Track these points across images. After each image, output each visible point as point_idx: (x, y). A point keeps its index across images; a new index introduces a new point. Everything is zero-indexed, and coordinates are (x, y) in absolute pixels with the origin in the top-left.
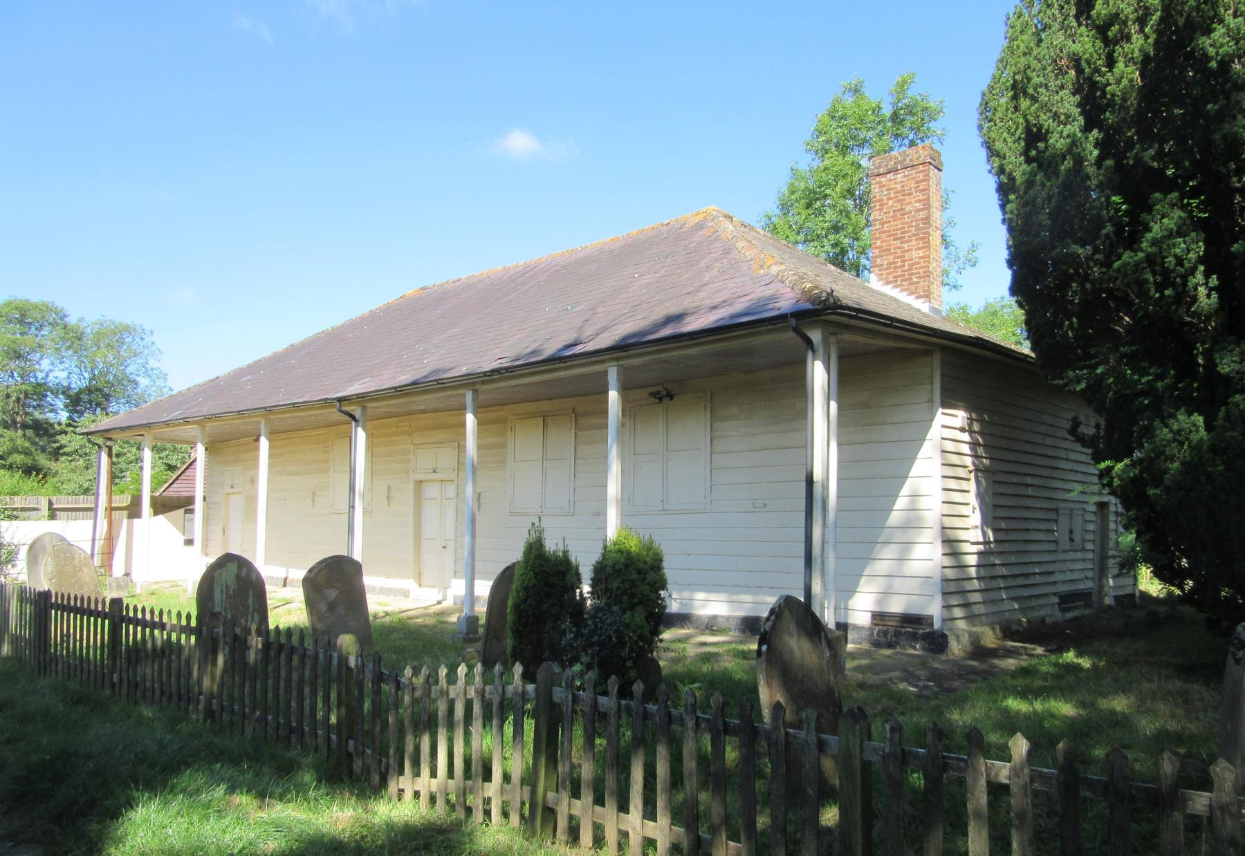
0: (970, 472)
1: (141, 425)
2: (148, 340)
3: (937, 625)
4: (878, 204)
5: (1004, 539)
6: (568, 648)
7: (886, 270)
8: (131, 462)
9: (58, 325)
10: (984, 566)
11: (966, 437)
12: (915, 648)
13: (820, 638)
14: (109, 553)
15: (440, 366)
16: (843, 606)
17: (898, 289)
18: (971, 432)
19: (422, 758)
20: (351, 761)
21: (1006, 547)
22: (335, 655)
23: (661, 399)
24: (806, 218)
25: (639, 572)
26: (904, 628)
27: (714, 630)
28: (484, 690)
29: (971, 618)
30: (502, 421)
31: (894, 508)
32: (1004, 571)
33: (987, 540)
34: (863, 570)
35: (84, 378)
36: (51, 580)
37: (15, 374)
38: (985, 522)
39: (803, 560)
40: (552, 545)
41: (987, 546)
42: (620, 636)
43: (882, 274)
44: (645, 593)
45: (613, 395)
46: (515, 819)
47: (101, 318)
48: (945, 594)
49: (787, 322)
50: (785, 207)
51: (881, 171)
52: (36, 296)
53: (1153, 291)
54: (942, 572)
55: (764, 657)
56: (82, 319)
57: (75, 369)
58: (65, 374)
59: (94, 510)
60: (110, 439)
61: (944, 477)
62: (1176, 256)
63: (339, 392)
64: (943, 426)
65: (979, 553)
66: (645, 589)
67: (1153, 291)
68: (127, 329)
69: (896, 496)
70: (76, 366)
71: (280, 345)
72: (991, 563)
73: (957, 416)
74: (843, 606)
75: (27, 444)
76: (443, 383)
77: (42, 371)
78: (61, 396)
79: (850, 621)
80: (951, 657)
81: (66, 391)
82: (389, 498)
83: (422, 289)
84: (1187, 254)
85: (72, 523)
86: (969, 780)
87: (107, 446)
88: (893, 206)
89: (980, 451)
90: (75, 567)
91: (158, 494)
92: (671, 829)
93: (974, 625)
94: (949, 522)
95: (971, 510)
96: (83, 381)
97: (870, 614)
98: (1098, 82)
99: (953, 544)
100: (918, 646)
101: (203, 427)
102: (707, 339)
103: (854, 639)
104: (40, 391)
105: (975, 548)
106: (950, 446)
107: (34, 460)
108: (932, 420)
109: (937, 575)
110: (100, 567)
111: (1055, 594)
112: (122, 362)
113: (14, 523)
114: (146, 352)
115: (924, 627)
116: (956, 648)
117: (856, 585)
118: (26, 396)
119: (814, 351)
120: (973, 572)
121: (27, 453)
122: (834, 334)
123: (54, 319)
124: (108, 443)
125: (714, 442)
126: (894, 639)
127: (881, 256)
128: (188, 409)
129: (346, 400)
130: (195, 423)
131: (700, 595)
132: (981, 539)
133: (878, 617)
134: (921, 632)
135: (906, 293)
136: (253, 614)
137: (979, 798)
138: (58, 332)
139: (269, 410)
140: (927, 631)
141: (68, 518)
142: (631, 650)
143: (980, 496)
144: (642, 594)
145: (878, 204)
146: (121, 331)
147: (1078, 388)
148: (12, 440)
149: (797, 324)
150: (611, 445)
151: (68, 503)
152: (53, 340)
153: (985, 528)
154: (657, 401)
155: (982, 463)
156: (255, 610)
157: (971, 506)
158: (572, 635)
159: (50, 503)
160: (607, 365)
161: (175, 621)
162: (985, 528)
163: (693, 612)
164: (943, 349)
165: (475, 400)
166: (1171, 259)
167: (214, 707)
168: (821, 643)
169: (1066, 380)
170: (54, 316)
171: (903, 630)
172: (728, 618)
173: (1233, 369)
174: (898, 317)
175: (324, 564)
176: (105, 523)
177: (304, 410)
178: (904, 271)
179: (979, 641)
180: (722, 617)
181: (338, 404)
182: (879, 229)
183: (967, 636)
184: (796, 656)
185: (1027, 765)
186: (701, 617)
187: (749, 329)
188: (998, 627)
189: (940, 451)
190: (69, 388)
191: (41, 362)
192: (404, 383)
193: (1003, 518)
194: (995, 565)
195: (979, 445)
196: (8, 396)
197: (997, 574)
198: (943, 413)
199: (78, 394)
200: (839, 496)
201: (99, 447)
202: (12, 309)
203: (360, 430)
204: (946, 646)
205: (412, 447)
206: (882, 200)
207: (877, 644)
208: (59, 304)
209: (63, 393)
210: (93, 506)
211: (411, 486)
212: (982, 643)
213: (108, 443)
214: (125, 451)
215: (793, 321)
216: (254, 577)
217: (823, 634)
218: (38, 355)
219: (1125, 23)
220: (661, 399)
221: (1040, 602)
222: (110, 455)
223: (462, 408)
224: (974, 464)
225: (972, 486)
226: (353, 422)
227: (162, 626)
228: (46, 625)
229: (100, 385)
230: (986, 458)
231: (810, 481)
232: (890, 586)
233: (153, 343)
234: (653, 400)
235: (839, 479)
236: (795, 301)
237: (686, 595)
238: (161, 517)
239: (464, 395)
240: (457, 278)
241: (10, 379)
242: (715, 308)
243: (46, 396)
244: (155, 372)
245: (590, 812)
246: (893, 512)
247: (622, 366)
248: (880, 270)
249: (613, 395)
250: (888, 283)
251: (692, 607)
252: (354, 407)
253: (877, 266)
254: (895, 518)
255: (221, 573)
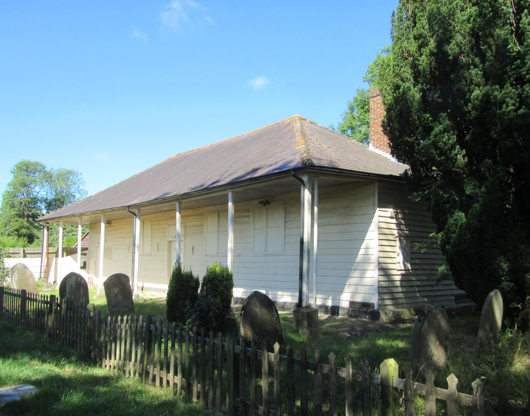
0: (396, 237)
1: (58, 217)
2: (80, 177)
3: (376, 308)
4: (373, 111)
5: (418, 268)
6: (187, 312)
7: (376, 141)
8: (68, 232)
9: (41, 171)
10: (405, 281)
11: (394, 221)
12: (366, 318)
13: (272, 309)
14: (47, 273)
15: (168, 192)
16: (338, 299)
17: (382, 150)
18: (397, 219)
19: (112, 352)
20: (91, 353)
21: (419, 272)
22: (87, 311)
23: (265, 204)
24: (361, 114)
25: (220, 281)
26: (362, 309)
27: (285, 309)
28: (131, 326)
29: (395, 305)
30: (202, 214)
31: (359, 254)
32: (418, 283)
33: (407, 268)
34: (346, 282)
35: (53, 195)
36: (17, 283)
37: (24, 194)
38: (405, 260)
39: (298, 277)
40: (185, 269)
41: (407, 272)
42: (209, 308)
43: (374, 144)
44: (222, 290)
45: (230, 204)
46: (137, 375)
47: (60, 168)
48: (379, 293)
49: (290, 173)
50: (352, 109)
51: (374, 95)
52: (33, 159)
53: (437, 157)
54: (378, 283)
55: (242, 316)
56: (52, 169)
57: (49, 191)
58: (45, 193)
59: (41, 253)
60: (48, 223)
61: (379, 239)
62: (443, 142)
63: (129, 203)
64: (379, 216)
65: (402, 275)
66: (222, 288)
67: (437, 157)
68: (70, 173)
69: (360, 248)
70: (50, 189)
71: (117, 181)
72: (410, 279)
73: (388, 211)
74: (338, 299)
75: (28, 225)
76: (151, 203)
77: (36, 192)
78: (43, 203)
79: (341, 305)
80: (381, 322)
81: (45, 200)
82: (158, 249)
83: (178, 155)
84: (449, 141)
85: (33, 259)
86: (263, 360)
87: (46, 226)
88: (379, 112)
89: (403, 227)
90: (27, 277)
91: (74, 246)
92: (182, 380)
93: (398, 308)
94: (382, 260)
95: (397, 255)
96: (52, 196)
97: (349, 302)
98: (482, 48)
99: (385, 270)
100: (367, 317)
101: (81, 218)
102: (266, 179)
103: (341, 313)
104: (35, 200)
105: (399, 273)
106: (383, 225)
107: (31, 231)
108: (374, 213)
109: (376, 285)
110: (44, 278)
111: (452, 295)
112: (69, 187)
113: (9, 259)
114: (79, 182)
115: (370, 308)
116: (384, 318)
117: (343, 289)
118: (29, 203)
119: (304, 185)
120: (398, 284)
121: (28, 229)
122: (315, 177)
123: (40, 169)
124: (47, 225)
125: (286, 224)
126: (358, 314)
127: (374, 135)
128: (75, 210)
129: (130, 207)
130: (78, 216)
131: (280, 293)
132: (403, 268)
133: (352, 303)
134: (368, 311)
135: (385, 152)
136: (82, 298)
137: (265, 367)
138: (42, 174)
139: (103, 211)
140: (372, 310)
141: (31, 257)
142: (214, 314)
143: (401, 247)
144: (220, 290)
145: (373, 111)
146: (68, 173)
147: (417, 200)
148: (22, 223)
149: (295, 174)
150: (229, 225)
151: (31, 251)
152: (39, 178)
153: (406, 263)
154: (263, 205)
155: (404, 233)
156: (83, 296)
157: (397, 253)
158: (189, 307)
159: (24, 251)
160: (228, 191)
161: (40, 299)
162: (406, 263)
163: (276, 300)
164: (379, 181)
165: (180, 206)
166: (441, 143)
167: (51, 333)
168: (272, 311)
169: (413, 197)
170: (40, 167)
171: (362, 310)
172: (291, 303)
173: (471, 192)
174: (345, 168)
175: (112, 277)
176: (46, 259)
177: (116, 211)
178: (384, 142)
179: (400, 316)
180: (288, 302)
181: (128, 208)
182: (373, 122)
183: (391, 313)
184: (259, 316)
185: (278, 354)
186: (280, 302)
187: (278, 175)
188: (413, 310)
189: (377, 228)
190: (47, 199)
191: (35, 188)
192: (152, 199)
193: (417, 259)
194: (413, 280)
195: (402, 224)
196: (21, 203)
197: (413, 285)
198: (379, 210)
199: (50, 202)
200: (318, 249)
201: (44, 227)
202: (23, 165)
203: (137, 219)
204: (379, 317)
205: (167, 226)
206: (375, 109)
207: (351, 316)
208: (42, 162)
209: (45, 201)
210: (41, 252)
211: (167, 243)
212: (402, 316)
213: (47, 225)
214: (66, 227)
215: (293, 172)
216: (83, 282)
217: (274, 307)
218: (34, 185)
219: (425, 38)
220: (265, 204)
221: (442, 298)
222: (48, 230)
223: (175, 210)
224: (398, 233)
225: (398, 243)
226: (135, 216)
227: (36, 300)
228: (2, 300)
229: (58, 198)
230: (406, 230)
231: (302, 242)
232: (357, 289)
233: (82, 178)
234: (261, 205)
235: (318, 241)
236: (297, 163)
237: (274, 292)
238: (69, 257)
239: (175, 204)
240: (192, 150)
241: (22, 196)
242: (270, 165)
243: (37, 203)
244: (82, 191)
245: (159, 373)
246: (359, 256)
247: (234, 191)
248: (374, 142)
249: (230, 204)
250: (377, 148)
251: (276, 298)
252: (135, 210)
253: (373, 140)
254: (359, 258)
255: (69, 280)
